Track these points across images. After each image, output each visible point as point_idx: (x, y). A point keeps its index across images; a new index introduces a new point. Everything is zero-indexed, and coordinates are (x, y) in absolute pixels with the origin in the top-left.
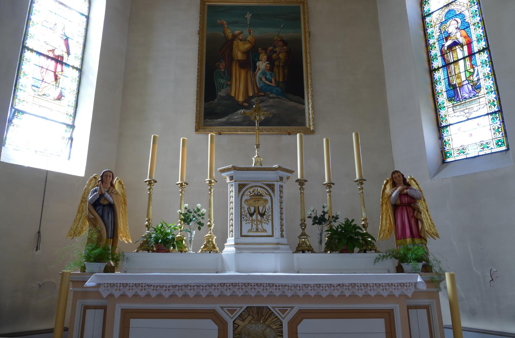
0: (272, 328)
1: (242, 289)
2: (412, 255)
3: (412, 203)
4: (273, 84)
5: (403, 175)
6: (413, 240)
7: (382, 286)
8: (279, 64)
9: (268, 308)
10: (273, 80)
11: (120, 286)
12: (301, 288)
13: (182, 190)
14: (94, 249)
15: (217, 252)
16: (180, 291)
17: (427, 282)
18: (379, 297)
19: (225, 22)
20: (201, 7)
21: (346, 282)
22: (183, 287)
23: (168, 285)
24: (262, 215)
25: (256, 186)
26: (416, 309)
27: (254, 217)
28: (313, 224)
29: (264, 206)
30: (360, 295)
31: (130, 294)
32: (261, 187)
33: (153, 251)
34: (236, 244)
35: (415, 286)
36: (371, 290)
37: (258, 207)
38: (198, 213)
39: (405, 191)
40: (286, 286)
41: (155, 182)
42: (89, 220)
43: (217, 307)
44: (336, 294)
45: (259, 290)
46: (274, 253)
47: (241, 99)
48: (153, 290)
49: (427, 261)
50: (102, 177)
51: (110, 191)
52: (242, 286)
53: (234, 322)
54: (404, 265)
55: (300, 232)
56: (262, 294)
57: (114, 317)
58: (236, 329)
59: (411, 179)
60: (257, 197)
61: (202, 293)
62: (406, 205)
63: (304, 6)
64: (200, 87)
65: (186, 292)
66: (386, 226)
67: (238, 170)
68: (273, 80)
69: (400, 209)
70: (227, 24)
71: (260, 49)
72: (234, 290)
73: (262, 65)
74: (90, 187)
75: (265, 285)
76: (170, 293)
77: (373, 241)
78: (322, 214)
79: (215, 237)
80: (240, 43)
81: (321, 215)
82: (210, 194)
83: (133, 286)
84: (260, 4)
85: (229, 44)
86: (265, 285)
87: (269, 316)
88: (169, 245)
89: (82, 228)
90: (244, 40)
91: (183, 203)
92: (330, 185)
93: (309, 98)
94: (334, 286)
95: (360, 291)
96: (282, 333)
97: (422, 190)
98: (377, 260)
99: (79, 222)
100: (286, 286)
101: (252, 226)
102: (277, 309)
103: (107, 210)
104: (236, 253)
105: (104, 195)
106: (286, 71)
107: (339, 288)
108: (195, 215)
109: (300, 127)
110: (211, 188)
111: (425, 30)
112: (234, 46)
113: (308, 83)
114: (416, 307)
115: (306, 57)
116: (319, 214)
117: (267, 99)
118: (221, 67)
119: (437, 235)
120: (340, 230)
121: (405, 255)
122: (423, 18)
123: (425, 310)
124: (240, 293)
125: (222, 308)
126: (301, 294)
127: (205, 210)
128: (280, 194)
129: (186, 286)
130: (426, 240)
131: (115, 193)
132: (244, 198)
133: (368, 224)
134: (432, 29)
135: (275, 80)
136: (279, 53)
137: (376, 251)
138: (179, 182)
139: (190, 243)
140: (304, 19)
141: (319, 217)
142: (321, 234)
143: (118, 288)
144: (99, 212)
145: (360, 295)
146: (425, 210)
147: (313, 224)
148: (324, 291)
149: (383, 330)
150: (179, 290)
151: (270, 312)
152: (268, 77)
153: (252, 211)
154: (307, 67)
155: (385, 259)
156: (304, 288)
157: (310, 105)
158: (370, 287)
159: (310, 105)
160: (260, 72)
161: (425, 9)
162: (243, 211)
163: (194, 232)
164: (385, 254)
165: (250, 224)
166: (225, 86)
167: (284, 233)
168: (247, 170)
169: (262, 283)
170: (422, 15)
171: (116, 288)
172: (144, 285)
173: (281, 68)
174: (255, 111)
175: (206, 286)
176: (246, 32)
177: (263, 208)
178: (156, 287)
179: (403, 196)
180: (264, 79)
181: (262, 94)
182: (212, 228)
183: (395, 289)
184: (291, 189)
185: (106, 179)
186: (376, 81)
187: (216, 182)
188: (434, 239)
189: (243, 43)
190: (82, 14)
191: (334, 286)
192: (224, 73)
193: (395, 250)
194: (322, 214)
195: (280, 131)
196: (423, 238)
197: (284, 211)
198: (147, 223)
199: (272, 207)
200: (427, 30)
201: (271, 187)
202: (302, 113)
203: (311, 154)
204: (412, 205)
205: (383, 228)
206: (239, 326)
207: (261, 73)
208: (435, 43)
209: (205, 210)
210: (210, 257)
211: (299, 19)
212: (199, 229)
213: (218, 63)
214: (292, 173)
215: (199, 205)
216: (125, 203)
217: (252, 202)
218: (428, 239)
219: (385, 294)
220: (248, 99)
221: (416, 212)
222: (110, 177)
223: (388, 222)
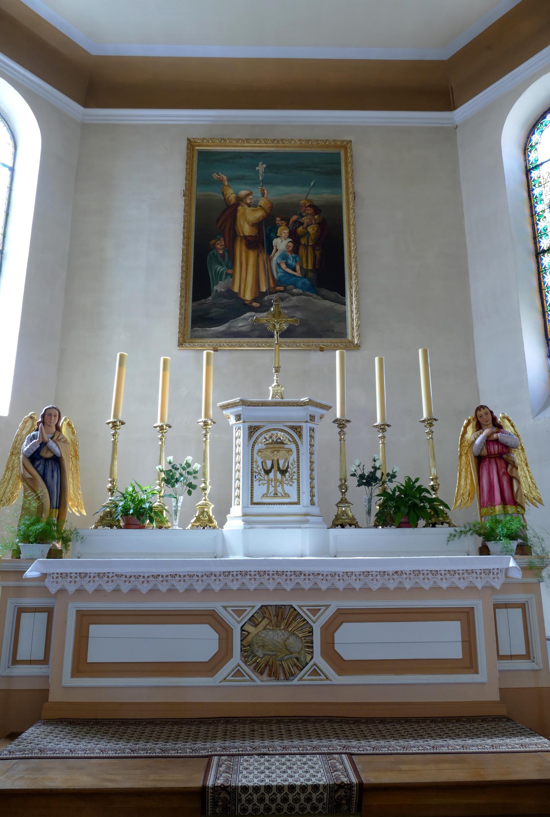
0: (297, 636)
1: (255, 579)
2: (503, 530)
3: (505, 453)
4: (298, 273)
5: (492, 413)
6: (504, 508)
7: (459, 574)
8: (308, 242)
9: (291, 606)
10: (298, 268)
11: (76, 577)
12: (341, 577)
13: (163, 436)
14: (33, 524)
15: (214, 528)
16: (164, 583)
17: (523, 569)
18: (454, 589)
19: (225, 178)
20: (187, 154)
21: (407, 568)
22: (169, 578)
23: (146, 575)
24: (283, 472)
25: (274, 429)
26: (506, 608)
27: (272, 475)
28: (359, 486)
29: (286, 459)
30: (427, 587)
31: (90, 587)
32: (282, 430)
33: (119, 527)
34: (244, 515)
35: (506, 574)
36: (442, 579)
37: (278, 460)
38: (188, 470)
39: (495, 436)
40: (319, 574)
41: (123, 423)
42: (24, 479)
43: (217, 606)
44: (392, 585)
45: (280, 581)
46: (300, 528)
47: (248, 296)
48: (125, 582)
49: (525, 538)
50: (43, 416)
51: (55, 438)
52: (255, 575)
53: (242, 627)
54: (491, 545)
55: (339, 497)
56: (285, 586)
57: (66, 622)
58: (245, 638)
59: (504, 417)
60: (277, 446)
61: (196, 586)
62: (496, 457)
63: (346, 152)
64: (187, 277)
65: (173, 585)
66: (466, 487)
67: (249, 406)
68: (298, 268)
69: (487, 463)
70: (228, 180)
71: (278, 219)
72: (244, 580)
73: (281, 243)
74: (24, 432)
75: (289, 573)
76: (150, 586)
77: (446, 510)
78: (372, 470)
79: (213, 506)
80: (248, 210)
81: (371, 472)
82: (205, 442)
83: (94, 577)
84: (279, 149)
85: (231, 211)
86: (289, 573)
87: (294, 619)
88: (144, 518)
89: (12, 493)
90: (254, 205)
91: (163, 456)
92: (383, 427)
93: (352, 295)
94: (388, 575)
95: (426, 581)
96: (312, 643)
97: (519, 434)
98: (452, 536)
99: (8, 484)
100: (319, 574)
101: (268, 489)
102: (305, 609)
103: (50, 466)
104: (245, 528)
105: (46, 444)
106: (318, 253)
107: (395, 576)
108: (184, 473)
109: (338, 340)
110: (207, 432)
111: (530, 191)
112: (239, 214)
113: (351, 271)
114: (506, 606)
115: (349, 232)
116: (368, 470)
117: (287, 297)
118: (219, 246)
119: (540, 501)
120: (397, 493)
121: (493, 530)
122: (528, 172)
123: (519, 610)
124: (252, 586)
125: (225, 607)
126: (341, 586)
127: (199, 466)
128: (310, 441)
129: (173, 576)
130: (523, 508)
131: (63, 440)
132: (257, 447)
133: (439, 485)
134: (540, 189)
135: (301, 268)
136: (308, 226)
137: (450, 525)
138: (159, 423)
139: (176, 514)
140: (347, 173)
141: (367, 474)
142: (370, 501)
143: (73, 579)
144: (39, 469)
145: (427, 587)
146: (524, 464)
147: (359, 486)
148: (375, 582)
149: (458, 637)
150: (162, 581)
151: (295, 613)
152: (290, 262)
153: (269, 467)
154: (350, 248)
155: (463, 536)
156: (346, 577)
157: (354, 306)
158: (441, 575)
159: (354, 306)
160: (278, 254)
161: (530, 158)
162: (255, 466)
163: (181, 499)
164: (463, 529)
165: (266, 485)
166: (224, 276)
167: (315, 499)
168: (262, 406)
169: (285, 570)
170: (526, 167)
171: (69, 579)
172: (110, 575)
173: (309, 247)
174: (274, 316)
175: (202, 576)
176: (257, 192)
177: (285, 461)
178: (128, 578)
179: (491, 444)
180: (283, 266)
181: (281, 288)
182: (208, 492)
183: (477, 578)
184: (326, 432)
185: (50, 419)
186: (456, 270)
187: (214, 423)
188: (536, 506)
189: (253, 210)
190: (4, 165)
191: (388, 575)
192: (223, 256)
193: (479, 523)
194: (372, 470)
195: (308, 346)
196: (519, 505)
197: (315, 466)
198: (110, 485)
199: (298, 460)
200: (533, 190)
201: (298, 430)
202: (342, 317)
203: (359, 380)
204: (505, 456)
205: (462, 491)
206: (249, 633)
207: (280, 256)
208: (544, 211)
209: (199, 466)
210: (206, 534)
211: (339, 172)
212: (190, 493)
213: (213, 241)
214: (328, 410)
215: (189, 459)
216: (76, 456)
217: (268, 453)
218: (526, 507)
219: (462, 585)
220: (259, 296)
221: (510, 467)
222: (55, 416)
223: (469, 481)
